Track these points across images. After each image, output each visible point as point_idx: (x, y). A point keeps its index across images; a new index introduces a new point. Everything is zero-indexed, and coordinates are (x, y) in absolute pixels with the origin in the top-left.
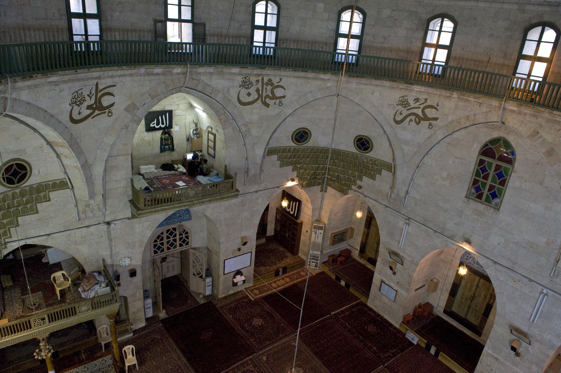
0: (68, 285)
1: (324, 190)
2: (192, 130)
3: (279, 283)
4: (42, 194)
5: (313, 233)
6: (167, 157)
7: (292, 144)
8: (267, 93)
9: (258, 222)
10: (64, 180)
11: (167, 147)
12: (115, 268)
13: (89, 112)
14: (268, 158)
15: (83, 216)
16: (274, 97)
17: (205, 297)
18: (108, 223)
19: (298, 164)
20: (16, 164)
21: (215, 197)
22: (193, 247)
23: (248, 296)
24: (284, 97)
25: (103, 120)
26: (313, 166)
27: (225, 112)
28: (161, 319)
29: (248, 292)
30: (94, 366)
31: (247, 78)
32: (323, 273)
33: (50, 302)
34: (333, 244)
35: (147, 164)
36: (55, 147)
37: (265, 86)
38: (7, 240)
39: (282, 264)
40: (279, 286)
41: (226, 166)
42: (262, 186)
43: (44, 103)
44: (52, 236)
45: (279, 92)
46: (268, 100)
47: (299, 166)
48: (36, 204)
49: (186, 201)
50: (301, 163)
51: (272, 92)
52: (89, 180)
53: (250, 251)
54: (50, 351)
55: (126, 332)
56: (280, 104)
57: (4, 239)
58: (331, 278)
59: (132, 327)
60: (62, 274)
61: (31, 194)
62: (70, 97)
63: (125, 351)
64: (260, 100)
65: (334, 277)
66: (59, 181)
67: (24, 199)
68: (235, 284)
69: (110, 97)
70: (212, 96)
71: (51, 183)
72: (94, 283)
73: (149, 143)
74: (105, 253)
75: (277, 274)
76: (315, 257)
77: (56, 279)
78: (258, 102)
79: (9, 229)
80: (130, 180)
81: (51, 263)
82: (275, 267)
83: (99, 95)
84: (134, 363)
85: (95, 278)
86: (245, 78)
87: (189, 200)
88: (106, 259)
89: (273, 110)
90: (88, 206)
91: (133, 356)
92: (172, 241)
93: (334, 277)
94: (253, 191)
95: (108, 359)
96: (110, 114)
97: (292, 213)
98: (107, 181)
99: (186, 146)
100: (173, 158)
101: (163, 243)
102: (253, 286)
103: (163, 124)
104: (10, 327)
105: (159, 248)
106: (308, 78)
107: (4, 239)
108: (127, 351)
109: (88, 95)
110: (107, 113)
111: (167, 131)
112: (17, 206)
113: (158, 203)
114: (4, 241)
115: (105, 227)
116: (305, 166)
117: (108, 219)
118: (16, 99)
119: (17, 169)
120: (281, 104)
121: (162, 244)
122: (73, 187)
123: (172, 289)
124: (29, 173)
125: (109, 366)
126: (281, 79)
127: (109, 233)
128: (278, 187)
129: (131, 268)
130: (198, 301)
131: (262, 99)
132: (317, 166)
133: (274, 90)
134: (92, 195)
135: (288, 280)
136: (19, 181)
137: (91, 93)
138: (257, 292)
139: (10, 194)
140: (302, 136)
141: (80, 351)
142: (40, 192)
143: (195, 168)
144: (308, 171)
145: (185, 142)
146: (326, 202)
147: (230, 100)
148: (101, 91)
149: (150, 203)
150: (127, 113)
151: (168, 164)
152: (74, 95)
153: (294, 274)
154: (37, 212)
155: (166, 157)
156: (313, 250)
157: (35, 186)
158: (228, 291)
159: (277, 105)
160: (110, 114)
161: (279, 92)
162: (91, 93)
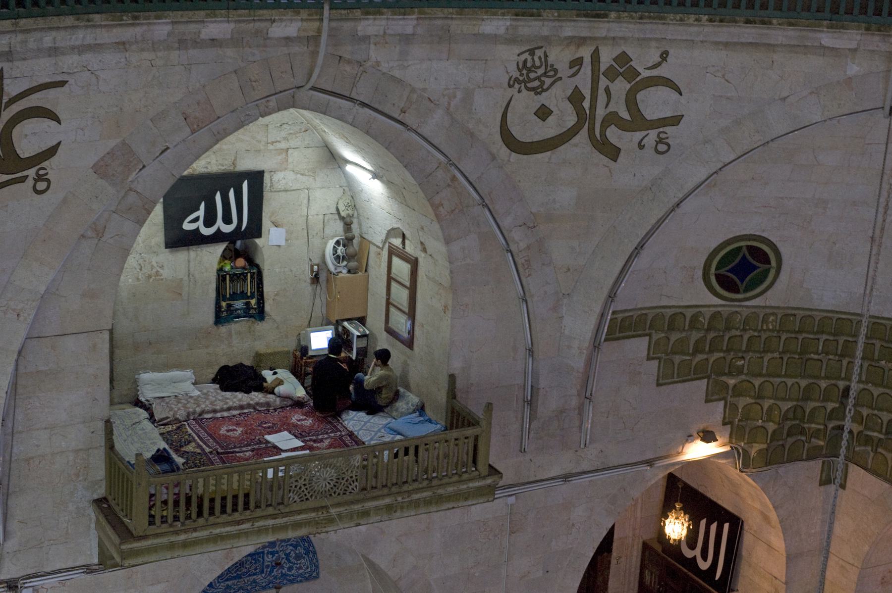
2: (331, 244)
6: (239, 343)
7: (702, 297)
8: (612, 108)
11: (239, 304)
14: (610, 351)
19: (730, 374)
21: (409, 493)
24: (676, 120)
26: (790, 382)
27: (454, 178)
31: (539, 53)
35: (166, 367)
37: (603, 82)
45: (655, 103)
46: (613, 134)
47: (732, 382)
49: (305, 505)
50: (740, 371)
64: (584, 132)
70: (409, 119)
73: (176, 289)
86: (532, 52)
87: (311, 504)
89: (636, 168)
97: (704, 566)
100: (261, 347)
103: (227, 220)
110: (30, 182)
111: (241, 246)
113: (200, 514)
116: (757, 382)
120: (663, 146)
126: (664, 56)
128: (650, 463)
131: (591, 130)
132: (803, 383)
133: (640, 96)
140: (743, 266)
143: (337, 384)
144: (767, 404)
147: (472, 135)
149: (169, 513)
151: (241, 365)
159: (649, 152)
161: (655, 103)
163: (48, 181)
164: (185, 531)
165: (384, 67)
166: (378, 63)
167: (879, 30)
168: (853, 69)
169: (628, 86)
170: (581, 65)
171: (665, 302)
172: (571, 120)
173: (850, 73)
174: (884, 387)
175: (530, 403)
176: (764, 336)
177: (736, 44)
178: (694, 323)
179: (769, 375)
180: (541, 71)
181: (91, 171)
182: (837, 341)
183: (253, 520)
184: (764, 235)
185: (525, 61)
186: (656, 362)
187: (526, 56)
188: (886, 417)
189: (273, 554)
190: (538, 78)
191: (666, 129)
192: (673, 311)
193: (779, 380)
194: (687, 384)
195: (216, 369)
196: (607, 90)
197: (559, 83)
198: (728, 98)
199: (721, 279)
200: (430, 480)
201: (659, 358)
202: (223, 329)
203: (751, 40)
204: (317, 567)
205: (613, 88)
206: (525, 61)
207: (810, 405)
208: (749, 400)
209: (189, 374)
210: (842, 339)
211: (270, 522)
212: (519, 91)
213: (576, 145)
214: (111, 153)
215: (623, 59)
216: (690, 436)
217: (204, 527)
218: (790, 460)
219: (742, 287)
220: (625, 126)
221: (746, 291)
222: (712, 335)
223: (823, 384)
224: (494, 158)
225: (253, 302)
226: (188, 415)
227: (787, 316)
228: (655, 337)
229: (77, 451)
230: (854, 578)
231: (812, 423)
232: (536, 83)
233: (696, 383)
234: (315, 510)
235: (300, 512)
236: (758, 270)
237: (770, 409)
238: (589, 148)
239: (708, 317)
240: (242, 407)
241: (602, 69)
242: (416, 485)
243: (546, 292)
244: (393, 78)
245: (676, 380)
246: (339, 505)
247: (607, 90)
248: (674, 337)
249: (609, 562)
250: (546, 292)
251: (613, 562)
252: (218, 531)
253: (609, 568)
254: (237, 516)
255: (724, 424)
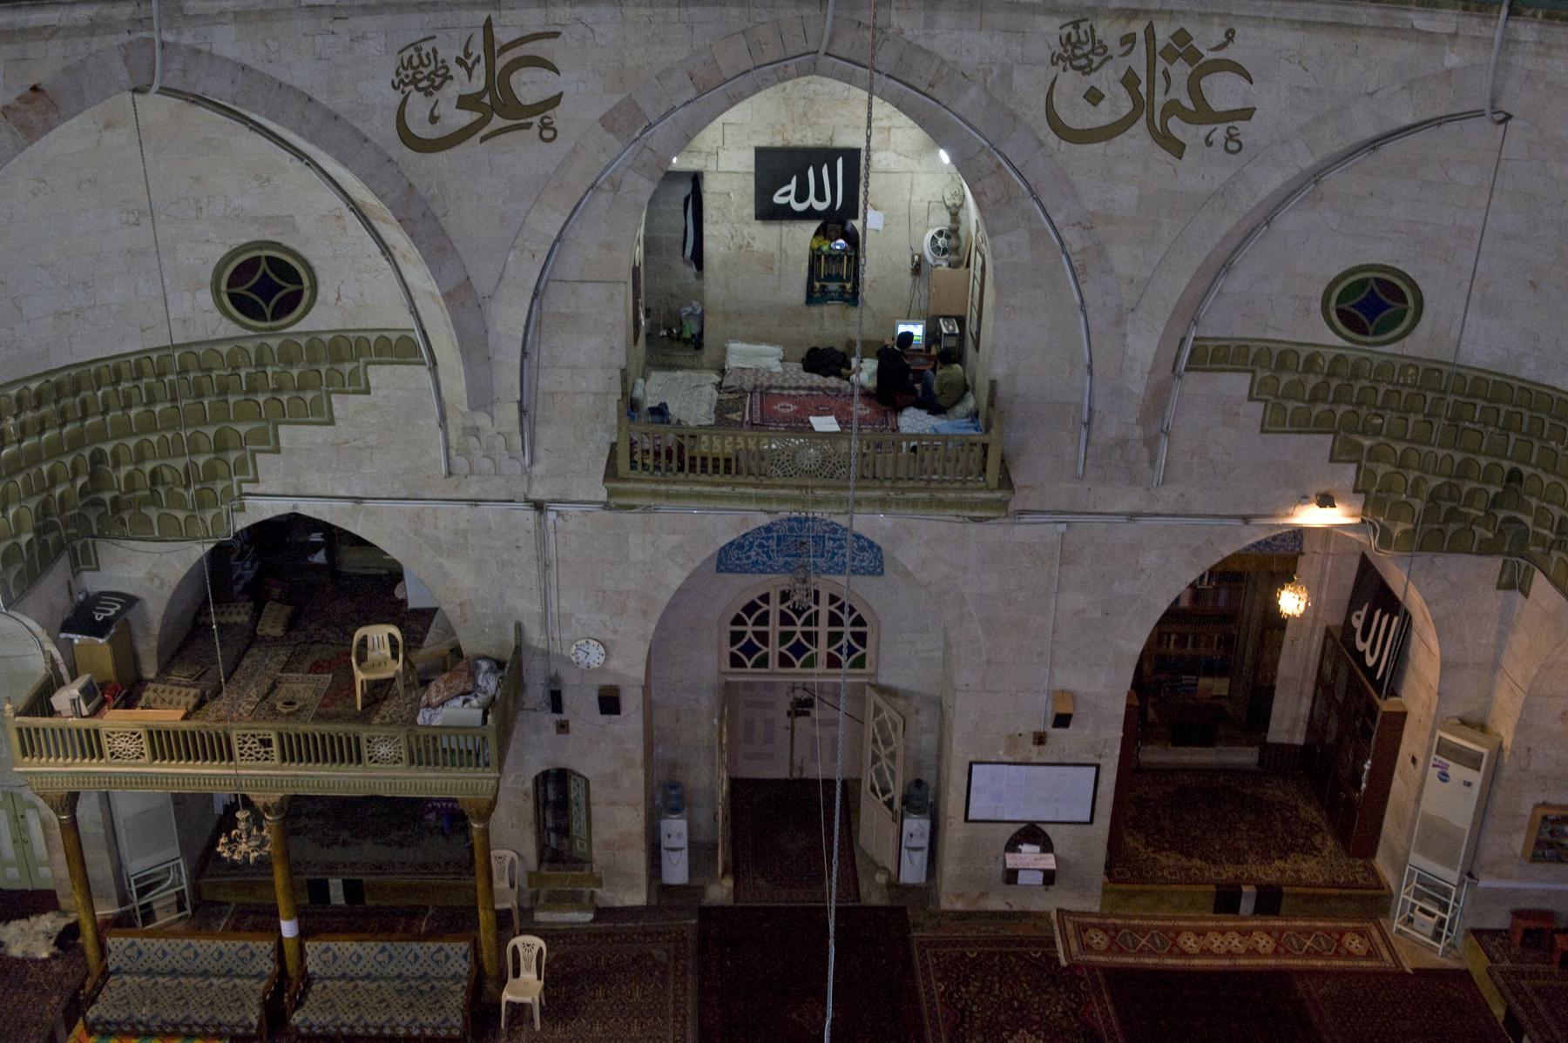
0: (390, 674)
1: (1515, 583)
2: (932, 232)
3: (1216, 942)
4: (347, 367)
5: (1433, 772)
6: (830, 326)
7: (1325, 337)
8: (1172, 95)
9: (1136, 647)
10: (410, 335)
11: (833, 286)
12: (555, 665)
13: (467, 118)
14: (1196, 384)
15: (460, 463)
16: (1203, 113)
17: (894, 886)
18: (539, 506)
19: (1364, 433)
20: (268, 258)
21: (904, 490)
22: (882, 681)
23: (1053, 943)
24: (1246, 114)
25: (521, 154)
26: (1441, 453)
27: (999, 166)
28: (705, 903)
29: (1063, 930)
30: (411, 957)
31: (1084, 26)
32: (1463, 976)
33: (332, 709)
34: (1535, 858)
35: (756, 340)
36: (374, 223)
37: (1161, 64)
38: (246, 488)
39: (1272, 872)
40: (1206, 953)
41: (993, 383)
42: (1168, 497)
43: (301, 73)
44: (368, 504)
45: (1222, 92)
46: (1176, 126)
48: (329, 394)
49: (789, 481)
50: (1377, 432)
51: (1194, 90)
52: (475, 346)
53: (1091, 759)
54: (260, 847)
55: (572, 899)
56: (1233, 146)
57: (240, 483)
58: (1483, 1010)
59: (598, 891)
60: (391, 636)
61: (313, 361)
62: (392, 63)
63: (515, 948)
64: (1142, 122)
65: (1499, 1012)
66: (378, 334)
67: (295, 372)
68: (1011, 876)
69: (545, 73)
70: (936, 93)
71: (373, 337)
72: (460, 689)
73: (767, 262)
74: (526, 607)
75: (1227, 901)
76: (1434, 892)
77: (370, 644)
78: (1134, 129)
79: (253, 453)
80: (618, 372)
81: (412, 605)
82: (1228, 872)
83: (500, 63)
84: (528, 1000)
85: (472, 676)
86: (1076, 25)
87: (795, 481)
88: (525, 623)
89: (1203, 170)
90: (475, 431)
91: (539, 978)
92: (798, 635)
93: (1499, 1012)
94: (1118, 509)
95: (454, 955)
96: (548, 133)
97: (1370, 661)
98: (543, 362)
99: (906, 294)
100: (854, 333)
101: (766, 634)
102: (1099, 915)
103: (820, 196)
104: (184, 734)
105: (750, 649)
106: (1356, 29)
107: (240, 483)
108: (521, 950)
109: (459, 61)
110: (535, 129)
111: (838, 222)
112: (274, 390)
113: (681, 469)
114: (240, 487)
115: (531, 515)
116: (1399, 447)
117: (538, 493)
118: (199, 52)
119: (269, 272)
120: (1234, 146)
121: (763, 637)
122: (435, 364)
123: (781, 819)
124: (307, 294)
125: (455, 977)
126: (1230, 35)
127: (542, 542)
128: (1246, 519)
129: (608, 681)
130: (863, 891)
131: (1150, 121)
132: (1458, 457)
133: (1204, 83)
134: (482, 399)
135: (1264, 943)
136: (277, 315)
137: (468, 55)
138: (1099, 940)
139: (250, 346)
140: (1373, 302)
141: (427, 908)
142: (342, 361)
143: (905, 378)
144: (1412, 475)
145: (907, 278)
146: (1519, 642)
147: (1015, 117)
148: (505, 49)
149: (649, 461)
150: (609, 136)
151: (831, 349)
152: (406, 55)
153: (1309, 932)
154: (331, 422)
155: (827, 324)
156: (1424, 851)
157: (327, 338)
158: (983, 895)
159: (1217, 149)
160: (548, 133)
161: (1222, 92)
162: (468, 55)
163: (555, 131)
164: (666, 482)
165: (908, 35)
166: (901, 31)
167: (1479, 10)
168: (1452, 59)
169: (1190, 70)
170: (1134, 42)
171: (1270, 335)
172: (1126, 106)
173: (1448, 64)
174: (1555, 474)
175: (1088, 424)
176: (1405, 391)
177: (1313, 24)
178: (1311, 362)
179: (1411, 441)
180: (1088, 48)
181: (598, 125)
182: (1376, 390)
183: (734, 485)
184: (1400, 267)
185: (1069, 36)
186: (1259, 406)
187: (1069, 29)
188: (1557, 512)
189: (834, 540)
190: (1086, 56)
191: (1236, 124)
192: (1283, 347)
193: (1427, 449)
194: (1303, 437)
195: (807, 349)
196: (1166, 74)
197: (1109, 63)
198: (1306, 90)
199: (1342, 314)
200: (929, 481)
201: (1267, 401)
202: (815, 310)
203: (1330, 19)
204: (881, 563)
205: (1172, 70)
206: (1069, 36)
207: (1467, 486)
208: (1389, 468)
209: (777, 350)
210: (1382, 389)
211: (752, 491)
212: (1065, 70)
213: (1133, 137)
214: (617, 108)
215: (1182, 37)
216: (1305, 497)
217: (684, 482)
218: (1453, 549)
219: (1371, 329)
220: (1189, 118)
221: (1375, 334)
222: (1334, 383)
223: (1484, 461)
224: (1041, 144)
225: (848, 286)
226: (755, 387)
227: (1431, 374)
228: (1259, 376)
229: (597, 394)
230: (1520, 704)
231: (1471, 506)
232: (1083, 62)
233: (1322, 437)
234: (798, 487)
235: (783, 487)
236: (1388, 311)
237: (1416, 483)
238: (1147, 140)
239: (1329, 358)
240: (811, 388)
241: (1158, 49)
242: (911, 484)
243: (1105, 305)
244: (920, 48)
245: (1287, 428)
246: (825, 487)
247: (1166, 74)
248: (1285, 378)
249: (1281, 642)
250: (1105, 305)
251: (1287, 642)
252: (698, 488)
253: (1280, 647)
254: (717, 478)
255: (1355, 491)
